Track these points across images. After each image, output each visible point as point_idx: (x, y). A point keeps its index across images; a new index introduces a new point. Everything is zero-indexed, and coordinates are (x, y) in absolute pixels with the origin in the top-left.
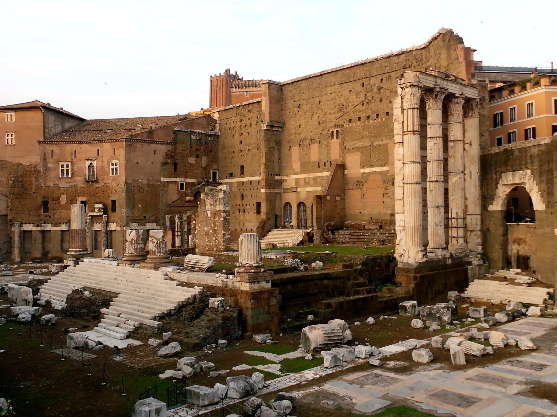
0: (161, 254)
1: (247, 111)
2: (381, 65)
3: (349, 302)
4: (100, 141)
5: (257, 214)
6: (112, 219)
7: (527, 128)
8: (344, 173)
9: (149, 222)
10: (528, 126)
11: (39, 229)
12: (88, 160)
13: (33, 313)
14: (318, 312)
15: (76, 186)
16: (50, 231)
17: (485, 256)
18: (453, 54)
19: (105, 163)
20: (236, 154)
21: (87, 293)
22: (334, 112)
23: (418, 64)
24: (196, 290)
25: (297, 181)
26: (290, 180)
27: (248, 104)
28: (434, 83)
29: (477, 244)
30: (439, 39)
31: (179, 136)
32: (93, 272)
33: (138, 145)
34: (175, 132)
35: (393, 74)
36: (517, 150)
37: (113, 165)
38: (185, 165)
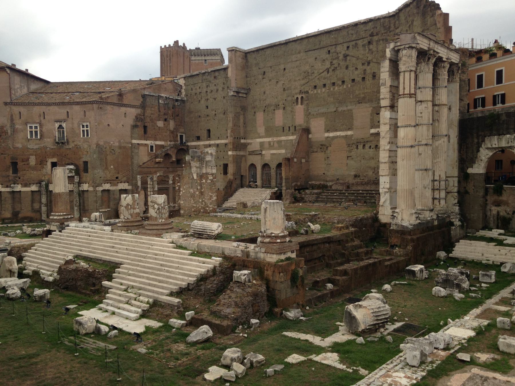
0: (163, 220)
1: (213, 78)
2: (348, 32)
3: (362, 268)
4: (70, 103)
5: (224, 174)
6: (84, 179)
7: (476, 97)
8: (308, 137)
9: (121, 183)
10: (496, 92)
11: (8, 189)
12: (57, 121)
13: (22, 286)
14: (334, 279)
15: (45, 148)
16: (20, 191)
17: (463, 217)
18: (429, 20)
19: (76, 125)
20: (203, 119)
21: (83, 264)
22: (299, 80)
23: (386, 31)
24: (216, 261)
25: (262, 144)
26: (255, 143)
27: (214, 71)
28: (428, 46)
29: (454, 205)
30: (411, 6)
31: (148, 100)
32: (84, 239)
33: (109, 107)
34: (144, 96)
35: (360, 42)
36: (504, 115)
37: (83, 126)
38: (154, 129)
